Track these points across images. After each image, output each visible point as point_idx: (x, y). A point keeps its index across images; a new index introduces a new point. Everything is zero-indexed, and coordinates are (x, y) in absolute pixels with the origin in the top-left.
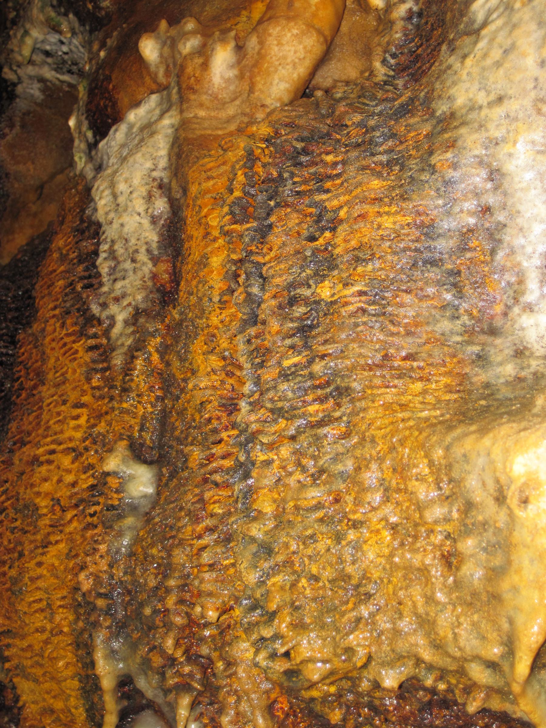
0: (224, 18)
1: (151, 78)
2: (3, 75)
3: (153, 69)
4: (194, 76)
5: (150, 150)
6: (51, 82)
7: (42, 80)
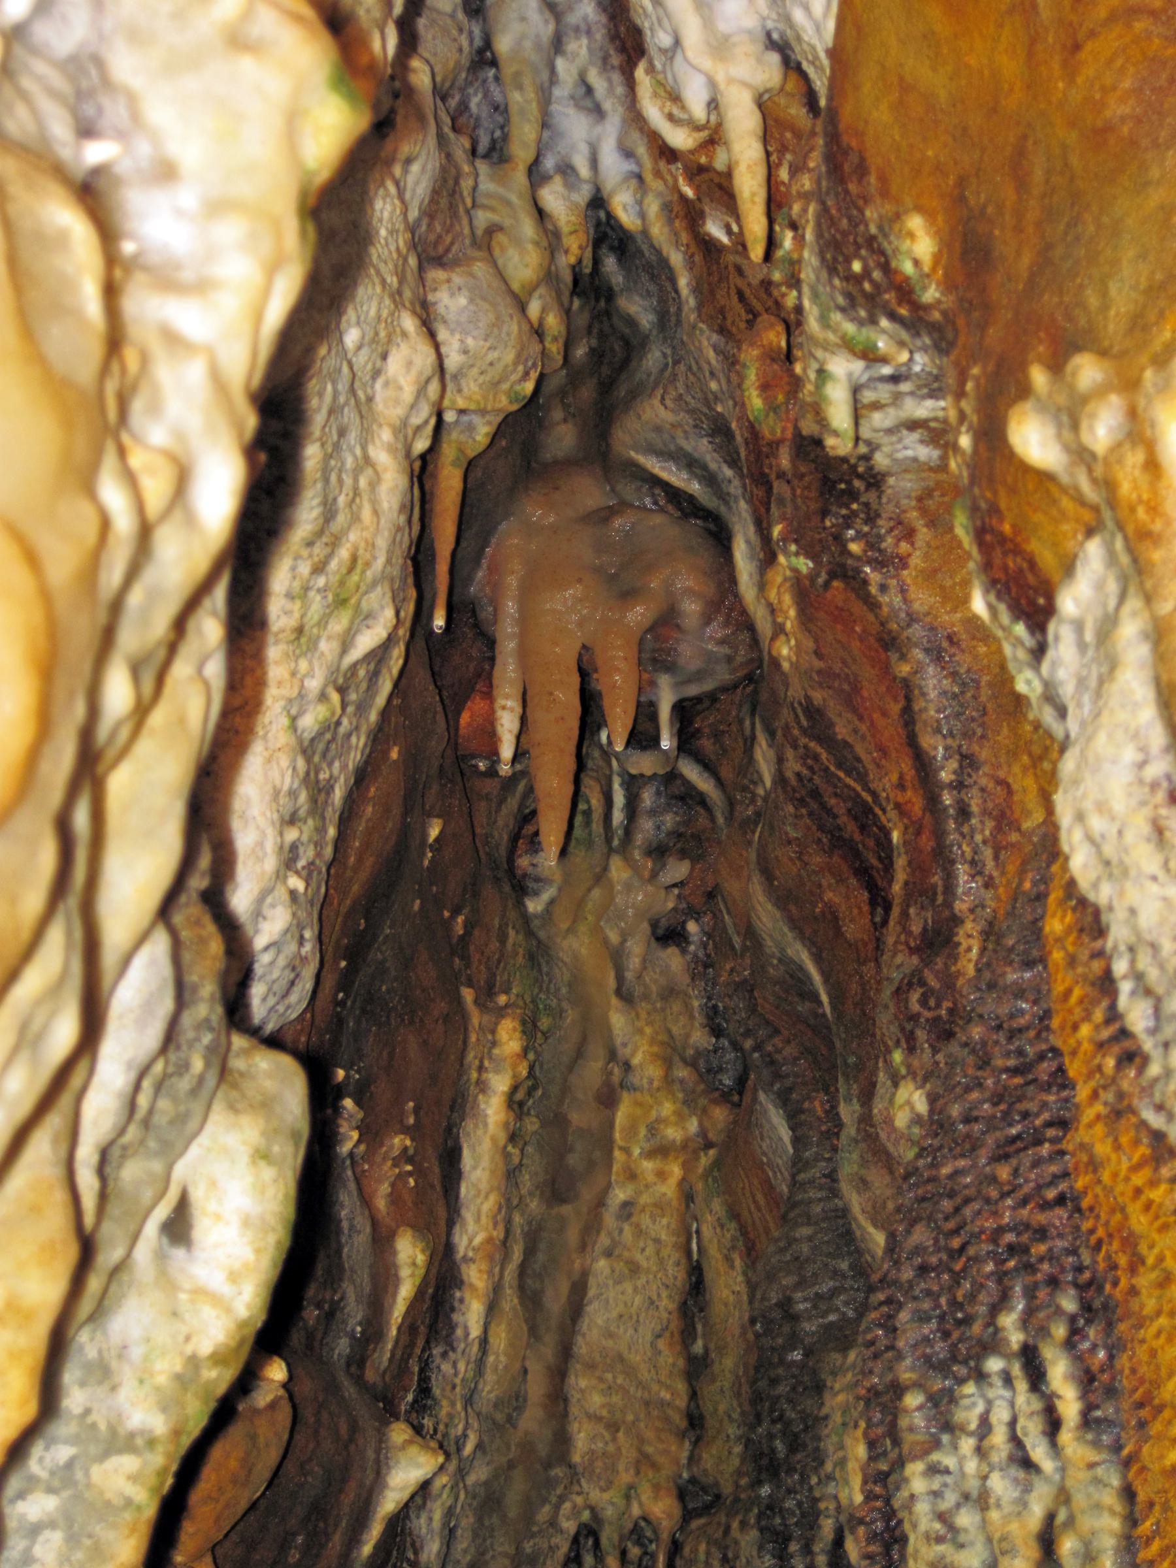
0: (1152, 317)
1: (1073, 498)
2: (832, 453)
3: (1065, 479)
4: (1140, 501)
5: (1122, 716)
6: (935, 419)
7: (913, 425)
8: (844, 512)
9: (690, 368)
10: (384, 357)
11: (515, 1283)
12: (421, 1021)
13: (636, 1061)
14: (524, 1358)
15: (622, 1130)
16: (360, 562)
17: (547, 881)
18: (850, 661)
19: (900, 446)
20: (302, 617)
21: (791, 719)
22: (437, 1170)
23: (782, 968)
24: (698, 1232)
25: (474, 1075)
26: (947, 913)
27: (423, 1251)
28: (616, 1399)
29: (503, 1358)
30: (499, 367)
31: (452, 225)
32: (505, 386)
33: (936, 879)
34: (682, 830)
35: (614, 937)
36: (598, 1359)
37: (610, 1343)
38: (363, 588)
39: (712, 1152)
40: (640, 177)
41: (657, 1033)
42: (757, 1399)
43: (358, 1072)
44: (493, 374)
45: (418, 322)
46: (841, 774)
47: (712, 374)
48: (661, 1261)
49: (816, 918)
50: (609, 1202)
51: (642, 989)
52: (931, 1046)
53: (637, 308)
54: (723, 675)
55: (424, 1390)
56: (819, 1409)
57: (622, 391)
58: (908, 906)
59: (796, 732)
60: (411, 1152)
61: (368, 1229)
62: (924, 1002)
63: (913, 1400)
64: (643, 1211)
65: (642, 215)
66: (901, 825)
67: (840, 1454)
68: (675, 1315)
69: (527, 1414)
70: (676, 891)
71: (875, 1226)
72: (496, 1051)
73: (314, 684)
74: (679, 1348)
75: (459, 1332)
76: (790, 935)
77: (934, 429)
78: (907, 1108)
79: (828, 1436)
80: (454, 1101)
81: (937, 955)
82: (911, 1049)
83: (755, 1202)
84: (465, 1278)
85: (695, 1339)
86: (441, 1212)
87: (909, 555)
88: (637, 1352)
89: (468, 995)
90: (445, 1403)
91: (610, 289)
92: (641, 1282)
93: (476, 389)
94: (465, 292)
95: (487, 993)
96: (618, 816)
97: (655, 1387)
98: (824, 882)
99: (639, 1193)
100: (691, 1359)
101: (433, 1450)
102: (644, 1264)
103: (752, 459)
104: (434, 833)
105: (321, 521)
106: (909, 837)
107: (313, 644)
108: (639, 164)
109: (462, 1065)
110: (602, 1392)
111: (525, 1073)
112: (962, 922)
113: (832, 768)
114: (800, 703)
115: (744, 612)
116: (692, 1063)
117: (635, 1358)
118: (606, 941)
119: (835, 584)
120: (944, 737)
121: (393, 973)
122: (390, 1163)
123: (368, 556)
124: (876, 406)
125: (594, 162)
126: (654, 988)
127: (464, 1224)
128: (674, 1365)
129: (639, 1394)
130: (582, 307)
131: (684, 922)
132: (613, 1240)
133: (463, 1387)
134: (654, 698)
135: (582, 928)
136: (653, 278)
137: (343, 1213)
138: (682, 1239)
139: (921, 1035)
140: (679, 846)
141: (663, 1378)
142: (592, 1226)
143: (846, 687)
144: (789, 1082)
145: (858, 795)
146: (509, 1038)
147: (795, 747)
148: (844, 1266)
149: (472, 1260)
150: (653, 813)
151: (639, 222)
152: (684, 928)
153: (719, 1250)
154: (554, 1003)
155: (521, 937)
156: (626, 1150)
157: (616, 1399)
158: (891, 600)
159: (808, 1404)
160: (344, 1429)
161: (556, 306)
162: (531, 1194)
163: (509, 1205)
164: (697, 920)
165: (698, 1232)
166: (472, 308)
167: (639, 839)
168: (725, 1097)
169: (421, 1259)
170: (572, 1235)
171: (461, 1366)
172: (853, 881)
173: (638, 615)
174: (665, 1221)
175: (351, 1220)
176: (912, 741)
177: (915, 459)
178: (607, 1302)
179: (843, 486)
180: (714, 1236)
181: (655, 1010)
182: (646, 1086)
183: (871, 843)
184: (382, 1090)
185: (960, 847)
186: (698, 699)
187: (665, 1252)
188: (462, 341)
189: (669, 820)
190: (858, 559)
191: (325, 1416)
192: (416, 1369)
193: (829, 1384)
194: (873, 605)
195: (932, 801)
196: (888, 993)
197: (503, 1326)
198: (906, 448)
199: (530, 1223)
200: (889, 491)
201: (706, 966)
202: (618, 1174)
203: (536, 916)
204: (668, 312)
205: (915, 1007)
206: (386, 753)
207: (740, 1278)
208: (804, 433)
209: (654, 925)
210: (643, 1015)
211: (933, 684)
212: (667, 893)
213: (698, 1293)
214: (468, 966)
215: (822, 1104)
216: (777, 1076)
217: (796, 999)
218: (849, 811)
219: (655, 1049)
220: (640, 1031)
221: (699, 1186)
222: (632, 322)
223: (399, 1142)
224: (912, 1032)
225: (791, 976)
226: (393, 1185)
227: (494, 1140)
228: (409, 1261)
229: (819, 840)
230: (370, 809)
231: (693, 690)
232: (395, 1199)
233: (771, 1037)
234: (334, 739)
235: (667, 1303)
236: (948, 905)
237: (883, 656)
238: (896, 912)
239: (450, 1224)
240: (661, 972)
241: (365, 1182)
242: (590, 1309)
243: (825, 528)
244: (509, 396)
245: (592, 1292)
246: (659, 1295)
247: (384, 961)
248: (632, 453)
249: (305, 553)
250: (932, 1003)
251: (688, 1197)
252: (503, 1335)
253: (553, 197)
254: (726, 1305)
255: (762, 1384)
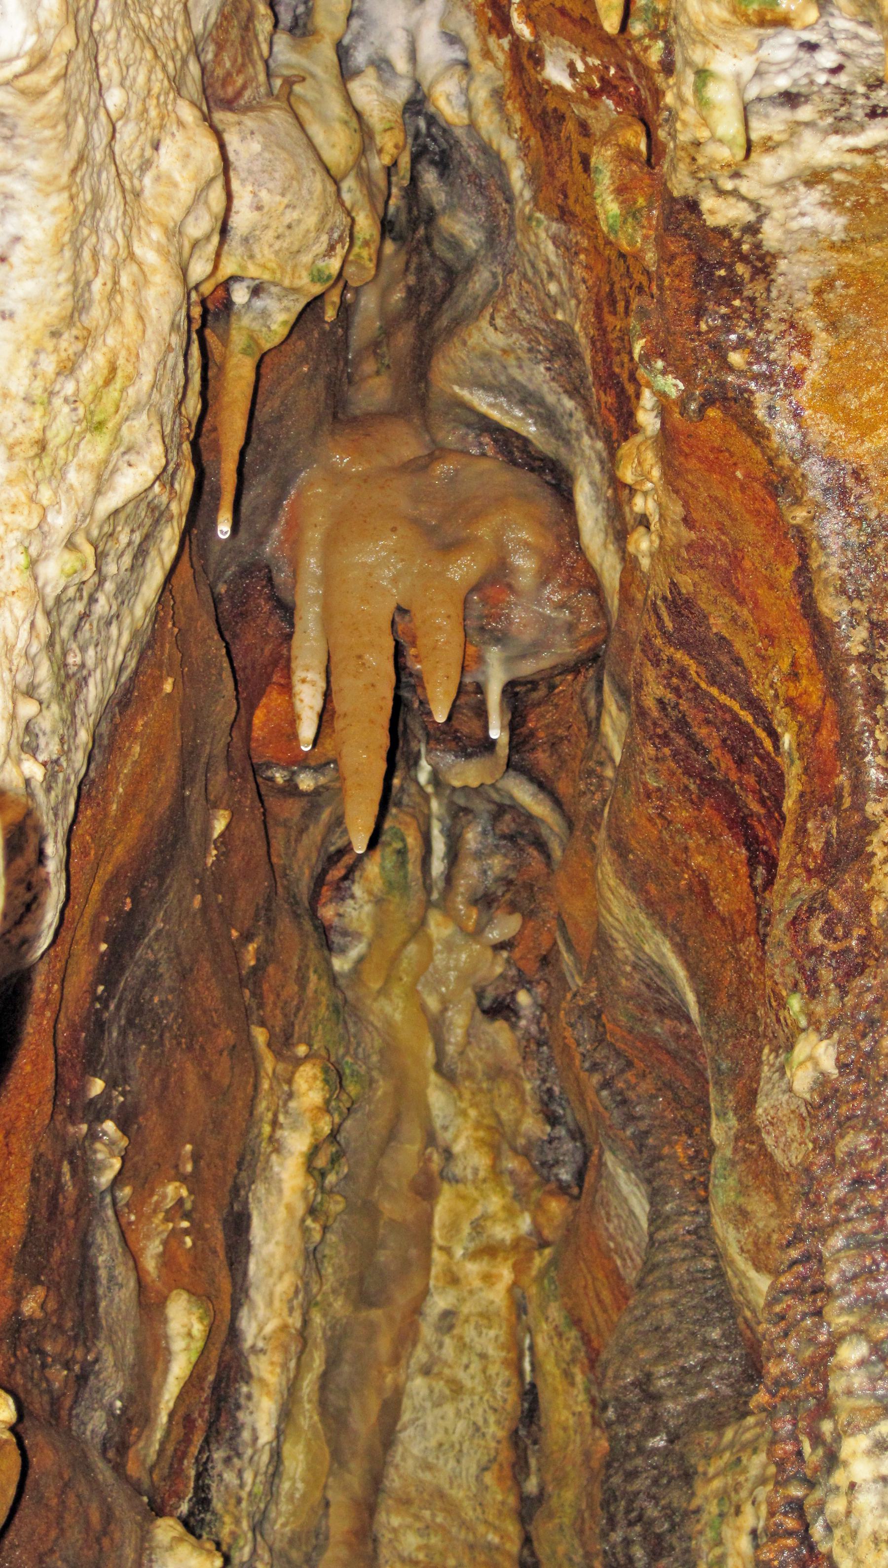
6: (841, 168)
7: (815, 177)
8: (724, 310)
9: (524, 276)
10: (156, 147)
11: (315, 1398)
12: (202, 1048)
13: (457, 1148)
14: (325, 1487)
15: (443, 1226)
16: (120, 373)
17: (357, 936)
18: (728, 523)
19: (795, 211)
20: (44, 430)
21: (652, 627)
22: (220, 1235)
23: (637, 977)
24: (531, 1348)
25: (267, 1129)
26: (857, 817)
27: (201, 1319)
28: (434, 1540)
29: (300, 1485)
30: (299, 231)
31: (244, 65)
32: (306, 258)
33: (842, 779)
34: (512, 875)
35: (433, 1003)
36: (413, 1494)
37: (427, 1476)
38: (123, 411)
39: (547, 1251)
40: (466, 65)
41: (483, 1116)
42: (610, 1498)
43: (124, 1093)
44: (290, 241)
45: (198, 114)
46: (714, 691)
47: (551, 275)
48: (488, 1381)
49: (680, 898)
50: (427, 1310)
51: (466, 1067)
52: (838, 986)
53: (463, 228)
54: (563, 650)
55: (202, 1501)
56: (689, 1501)
57: (444, 321)
58: (805, 821)
59: (658, 642)
60: (188, 1205)
61: (132, 1284)
62: (828, 932)
63: (852, 1352)
64: (467, 1321)
65: (469, 106)
66: (794, 726)
67: (718, 1551)
68: (505, 1445)
69: (329, 1555)
70: (505, 954)
71: (758, 1269)
72: (292, 1104)
73: (60, 522)
74: (509, 1483)
75: (246, 1435)
76: (647, 923)
77: (840, 184)
78: (809, 1065)
79: (701, 1533)
80: (243, 1158)
81: (845, 871)
82: (813, 993)
83: (600, 1301)
84: (254, 1371)
85: (528, 1475)
86: (225, 1285)
87: (805, 369)
88: (460, 1486)
89: (260, 1035)
90: (227, 1519)
91: (431, 209)
92: (464, 1405)
93: (272, 257)
94: (258, 137)
95: (283, 1043)
96: (438, 867)
97: (481, 1529)
98: (691, 843)
99: (462, 1300)
100: (523, 1499)
101: (209, 1552)
102: (468, 1384)
103: (599, 359)
104: (219, 826)
105: (70, 304)
106: (807, 735)
107: (59, 473)
108: (465, 48)
109: (251, 1114)
110: (420, 1532)
111: (327, 1130)
112: (877, 827)
113: (703, 685)
114: (664, 599)
115: (590, 570)
116: (525, 1153)
117: (458, 1494)
118: (423, 1008)
119: (712, 413)
120: (850, 599)
121: (167, 983)
122: (161, 1216)
123: (130, 369)
124: (770, 146)
125: (413, 55)
126: (479, 1066)
127: (253, 1307)
128: (503, 1503)
129: (462, 1535)
130: (397, 253)
131: (514, 993)
132: (431, 1355)
133: (251, 1503)
134: (481, 678)
135: (397, 990)
136: (481, 189)
137: (101, 1259)
138: (512, 1355)
139: (826, 974)
140: (508, 896)
141: (491, 1518)
142: (407, 1336)
143: (723, 562)
144: (643, 1125)
145: (736, 717)
146: (309, 1088)
147: (657, 663)
148: (715, 1334)
149: (263, 1351)
150: (478, 855)
151: (465, 114)
152: (514, 1000)
153: (557, 1364)
154: (363, 1070)
155: (324, 984)
156: (447, 1250)
157: (434, 1540)
158: (783, 428)
159: (675, 1497)
160: (95, 1517)
161: (368, 207)
162: (334, 1291)
163: (306, 1299)
164: (529, 990)
165: (531, 1348)
166: (267, 155)
167: (462, 885)
168: (563, 1189)
169: (198, 1329)
170: (384, 1345)
171: (248, 1476)
172: (727, 838)
173: (463, 569)
174: (492, 1333)
175: (111, 1269)
176: (809, 610)
177: (814, 232)
178: (424, 1427)
179: (722, 272)
180: (549, 1342)
181: (481, 1090)
182: (470, 1177)
183: (750, 779)
184: (152, 1122)
185: (872, 734)
186: (532, 684)
187: (493, 1370)
188: (255, 194)
189: (497, 864)
190: (741, 373)
191: (71, 1500)
192: (193, 1473)
193: (701, 1469)
194: (758, 434)
195: (835, 680)
196: (782, 926)
197: (300, 1447)
198: (803, 214)
199: (333, 1328)
200: (780, 280)
201: (539, 1044)
202: (437, 1278)
203: (342, 975)
204: (498, 226)
205: (817, 938)
206: (158, 682)
207: (582, 1397)
208: (676, 194)
209: (480, 995)
210: (467, 1095)
211: (833, 531)
212: (495, 956)
213: (531, 1422)
214: (261, 1006)
215: (686, 1148)
216: (632, 1118)
217: (654, 1018)
218: (724, 741)
219: (481, 1134)
220: (464, 1113)
221: (533, 1290)
222: (455, 245)
223: (173, 1191)
224: (814, 971)
225: (648, 986)
226: (165, 1243)
227: (289, 1208)
228: (184, 1330)
229: (686, 787)
230: (137, 749)
231: (527, 668)
232: (167, 1259)
233: (622, 1071)
234: (84, 616)
235: (495, 1430)
236: (858, 807)
237: (771, 506)
238: (789, 829)
239: (236, 1307)
240: (488, 1049)
241: (131, 1238)
242: (403, 1436)
243: (699, 333)
244: (311, 274)
245: (406, 1417)
246: (486, 1421)
247: (155, 964)
248: (456, 389)
249: (49, 344)
250: (839, 931)
251: (519, 1307)
252: (301, 1457)
253: (365, 92)
254: (565, 1429)
255: (616, 1480)
